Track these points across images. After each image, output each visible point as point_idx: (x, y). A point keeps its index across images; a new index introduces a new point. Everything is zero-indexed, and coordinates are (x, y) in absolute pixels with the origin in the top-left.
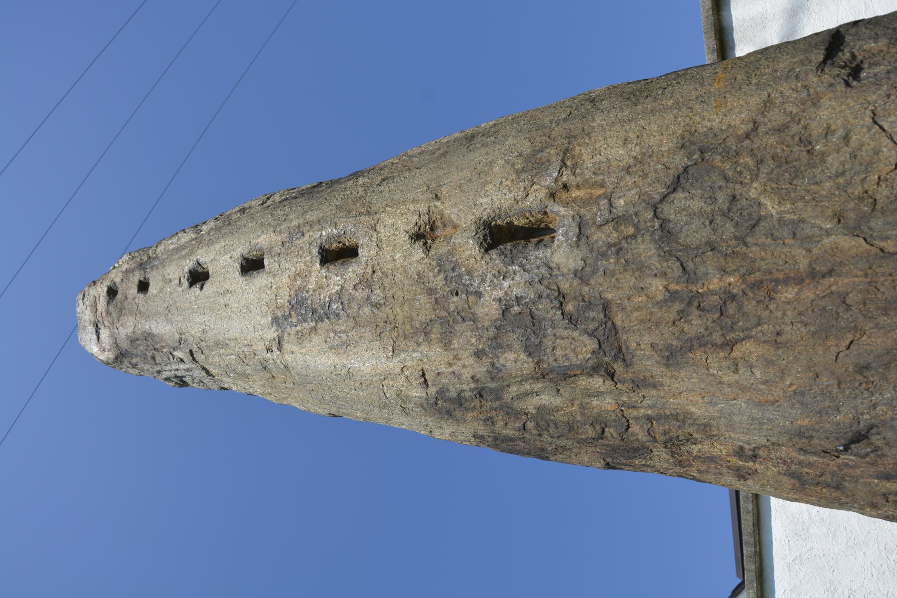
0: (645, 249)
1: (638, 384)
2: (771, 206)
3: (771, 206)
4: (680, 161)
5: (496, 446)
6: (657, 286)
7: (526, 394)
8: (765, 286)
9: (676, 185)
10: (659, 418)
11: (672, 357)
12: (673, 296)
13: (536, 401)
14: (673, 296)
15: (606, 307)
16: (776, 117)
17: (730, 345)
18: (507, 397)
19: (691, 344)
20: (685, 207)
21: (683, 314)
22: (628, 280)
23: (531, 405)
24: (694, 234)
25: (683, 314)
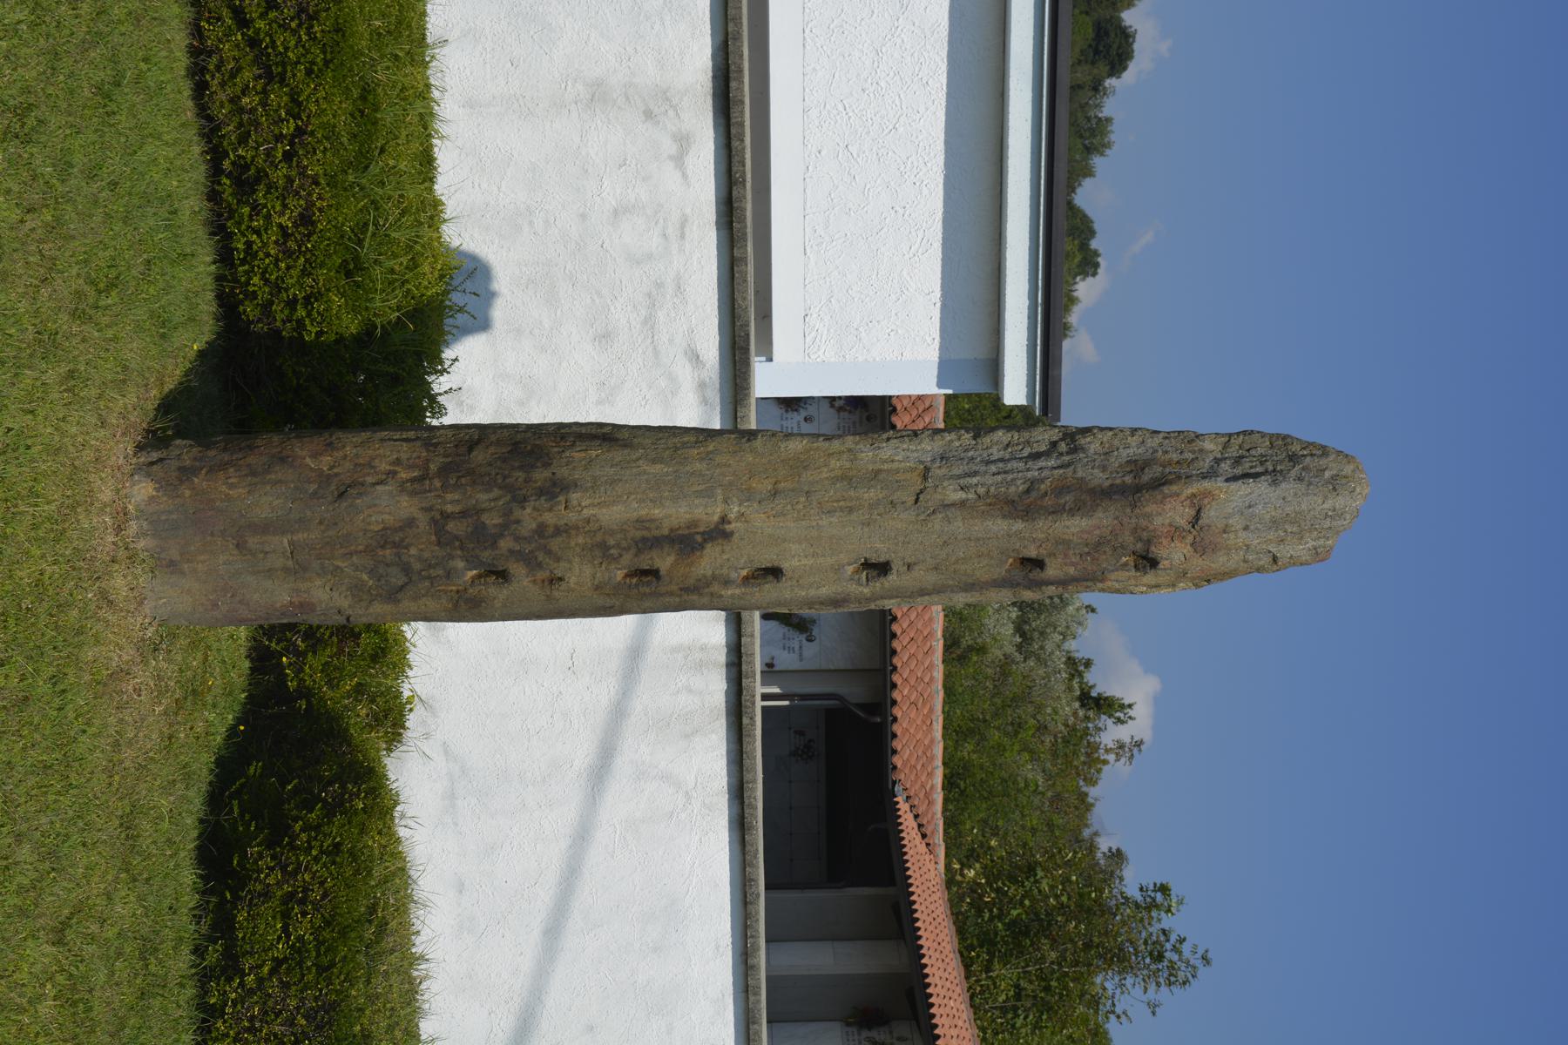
0: (417, 566)
1: (429, 509)
2: (365, 577)
3: (365, 577)
4: (399, 596)
5: (1324, 447)
6: (413, 551)
7: (495, 500)
8: (369, 550)
9: (401, 588)
10: (426, 491)
11: (411, 523)
12: (406, 548)
13: (492, 496)
14: (406, 548)
15: (439, 543)
16: (364, 604)
17: (385, 529)
18: (508, 497)
19: (401, 529)
20: (398, 579)
21: (402, 540)
22: (426, 555)
23: (496, 492)
24: (394, 570)
25: (402, 540)
